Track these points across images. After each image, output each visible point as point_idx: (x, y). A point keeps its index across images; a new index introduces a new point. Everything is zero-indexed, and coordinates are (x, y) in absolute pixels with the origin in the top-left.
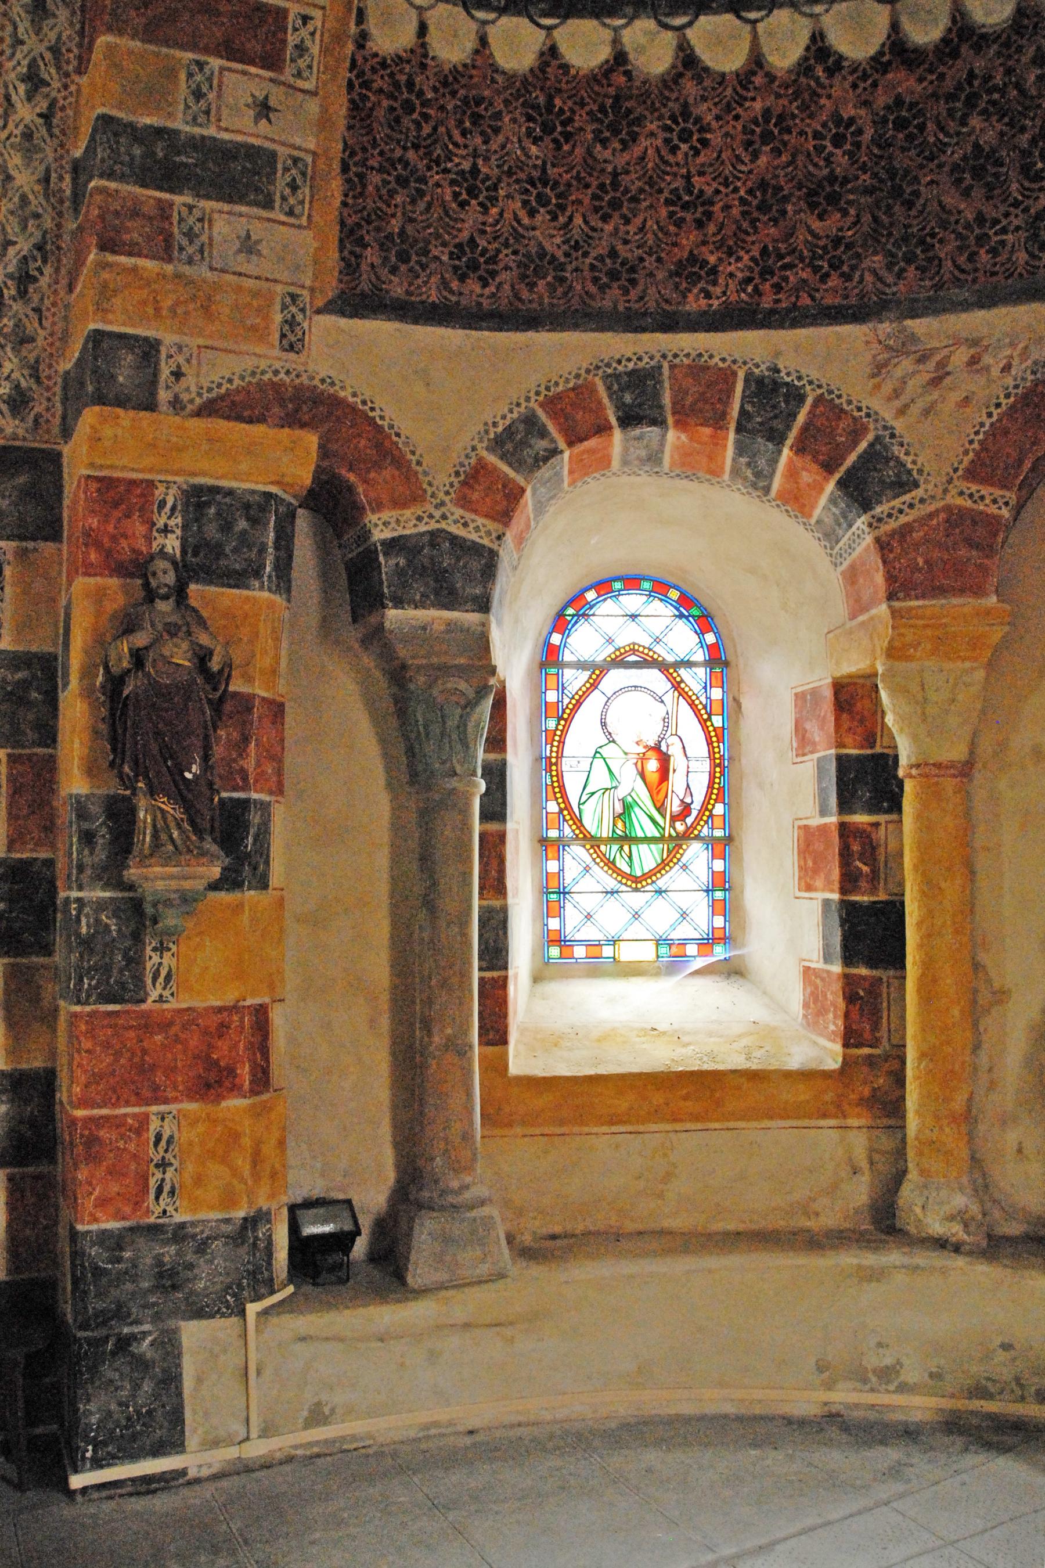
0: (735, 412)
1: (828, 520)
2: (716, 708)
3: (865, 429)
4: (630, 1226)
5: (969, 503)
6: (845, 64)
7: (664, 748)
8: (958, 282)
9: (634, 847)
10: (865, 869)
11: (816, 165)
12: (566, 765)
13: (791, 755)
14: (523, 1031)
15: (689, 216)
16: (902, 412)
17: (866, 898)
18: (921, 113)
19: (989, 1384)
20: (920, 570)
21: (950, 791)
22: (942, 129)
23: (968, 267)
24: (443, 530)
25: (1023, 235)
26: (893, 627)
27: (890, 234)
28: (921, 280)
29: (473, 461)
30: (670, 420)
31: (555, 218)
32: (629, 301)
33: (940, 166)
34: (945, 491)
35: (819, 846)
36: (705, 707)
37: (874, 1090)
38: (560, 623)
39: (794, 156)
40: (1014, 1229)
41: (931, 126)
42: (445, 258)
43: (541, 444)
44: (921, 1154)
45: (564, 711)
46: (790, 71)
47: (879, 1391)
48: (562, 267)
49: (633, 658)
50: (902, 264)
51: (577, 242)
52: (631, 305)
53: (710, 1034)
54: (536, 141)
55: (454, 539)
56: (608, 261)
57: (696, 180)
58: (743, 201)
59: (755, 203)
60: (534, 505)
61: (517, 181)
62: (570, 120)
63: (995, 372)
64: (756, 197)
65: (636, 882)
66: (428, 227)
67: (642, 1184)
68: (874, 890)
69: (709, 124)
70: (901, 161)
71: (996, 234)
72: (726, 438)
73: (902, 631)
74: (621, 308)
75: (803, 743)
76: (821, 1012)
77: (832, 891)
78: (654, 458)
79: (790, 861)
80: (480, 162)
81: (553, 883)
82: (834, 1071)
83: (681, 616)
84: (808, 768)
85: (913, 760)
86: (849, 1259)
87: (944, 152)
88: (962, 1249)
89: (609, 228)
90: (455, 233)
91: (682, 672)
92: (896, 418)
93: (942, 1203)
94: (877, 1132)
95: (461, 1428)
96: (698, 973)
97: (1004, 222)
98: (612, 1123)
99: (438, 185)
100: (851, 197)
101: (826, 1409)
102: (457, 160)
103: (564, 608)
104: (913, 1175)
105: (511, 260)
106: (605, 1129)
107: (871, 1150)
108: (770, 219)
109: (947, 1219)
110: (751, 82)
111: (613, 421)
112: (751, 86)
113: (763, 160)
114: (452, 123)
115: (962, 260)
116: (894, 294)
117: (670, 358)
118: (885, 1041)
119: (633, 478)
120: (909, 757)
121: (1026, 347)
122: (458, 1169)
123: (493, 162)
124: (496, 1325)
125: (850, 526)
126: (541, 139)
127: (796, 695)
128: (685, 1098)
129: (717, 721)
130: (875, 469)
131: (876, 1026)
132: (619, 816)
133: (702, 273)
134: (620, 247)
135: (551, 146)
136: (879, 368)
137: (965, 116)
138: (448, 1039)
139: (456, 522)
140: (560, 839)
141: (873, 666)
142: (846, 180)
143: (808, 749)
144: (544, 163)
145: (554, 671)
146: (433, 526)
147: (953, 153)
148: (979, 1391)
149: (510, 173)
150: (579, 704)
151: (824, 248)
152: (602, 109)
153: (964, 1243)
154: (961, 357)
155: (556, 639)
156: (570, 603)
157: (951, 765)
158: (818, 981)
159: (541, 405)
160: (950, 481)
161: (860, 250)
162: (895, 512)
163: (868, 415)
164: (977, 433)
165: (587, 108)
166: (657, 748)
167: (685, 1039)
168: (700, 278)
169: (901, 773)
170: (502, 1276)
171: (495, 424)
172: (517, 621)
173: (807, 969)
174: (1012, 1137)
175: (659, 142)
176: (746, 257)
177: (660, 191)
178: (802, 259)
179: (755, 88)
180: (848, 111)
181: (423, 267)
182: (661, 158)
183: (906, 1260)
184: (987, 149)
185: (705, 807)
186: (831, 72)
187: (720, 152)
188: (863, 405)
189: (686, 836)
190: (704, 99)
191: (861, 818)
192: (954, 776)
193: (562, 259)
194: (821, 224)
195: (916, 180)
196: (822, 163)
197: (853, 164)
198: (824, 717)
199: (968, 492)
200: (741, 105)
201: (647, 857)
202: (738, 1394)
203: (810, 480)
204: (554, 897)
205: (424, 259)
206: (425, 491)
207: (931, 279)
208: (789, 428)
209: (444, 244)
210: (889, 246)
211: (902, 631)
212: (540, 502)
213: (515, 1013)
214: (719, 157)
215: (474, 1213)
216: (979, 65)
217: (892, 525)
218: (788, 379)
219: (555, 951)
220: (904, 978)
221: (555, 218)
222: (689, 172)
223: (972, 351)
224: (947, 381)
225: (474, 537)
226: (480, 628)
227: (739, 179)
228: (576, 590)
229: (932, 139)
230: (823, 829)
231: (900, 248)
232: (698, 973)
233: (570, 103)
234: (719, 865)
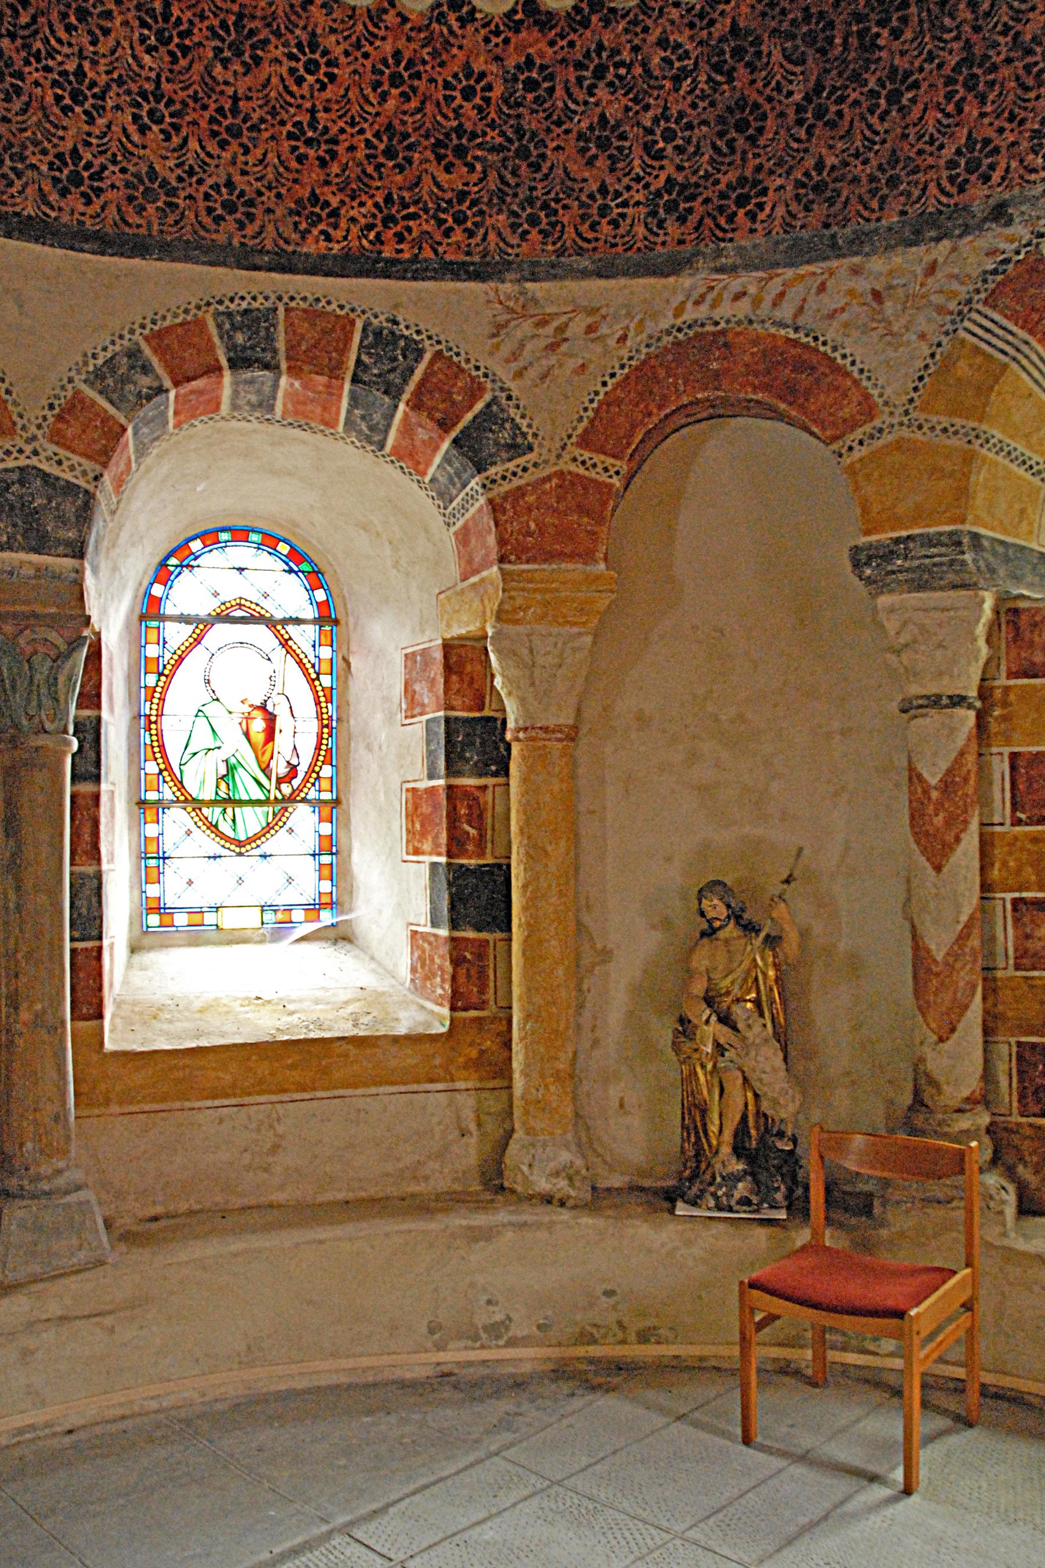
0: (351, 364)
1: (443, 480)
2: (325, 667)
3: (481, 389)
4: (237, 1202)
5: (581, 471)
6: (478, 16)
7: (270, 708)
8: (580, 252)
9: (237, 810)
10: (473, 832)
11: (445, 116)
12: (166, 723)
13: (400, 717)
14: (119, 1004)
15: (311, 153)
16: (519, 374)
17: (473, 862)
18: (551, 77)
19: (595, 1331)
20: (530, 534)
21: (556, 754)
22: (570, 95)
23: (590, 235)
24: (35, 468)
25: (643, 210)
26: (504, 591)
27: (515, 195)
28: (544, 244)
29: (69, 394)
30: (284, 366)
31: (168, 138)
32: (244, 237)
33: (567, 132)
34: (559, 456)
35: (426, 809)
36: (313, 666)
37: (482, 1052)
38: (163, 574)
39: (423, 103)
40: (617, 1181)
41: (559, 92)
42: (44, 168)
43: (145, 382)
44: (527, 1112)
45: (165, 667)
46: (421, 14)
47: (490, 1347)
48: (172, 192)
49: (239, 613)
50: (526, 226)
51: (191, 167)
52: (246, 241)
53: (317, 1002)
54: (149, 50)
55: (45, 476)
56: (224, 190)
57: (321, 115)
58: (368, 144)
59: (382, 147)
60: (136, 446)
61: (129, 92)
62: (188, 33)
63: (612, 342)
64: (382, 141)
65: (240, 845)
66: (25, 130)
67: (247, 1158)
68: (482, 854)
69: (337, 59)
70: (531, 123)
71: (617, 206)
72: (342, 387)
73: (513, 593)
74: (236, 242)
75: (413, 705)
76: (429, 977)
77: (439, 854)
78: (266, 405)
79: (398, 824)
80: (87, 65)
81: (152, 848)
82: (442, 1035)
83: (291, 571)
84: (418, 729)
85: (521, 723)
86: (459, 1220)
87: (571, 119)
88: (568, 1204)
89: (226, 155)
90: (55, 141)
91: (291, 628)
92: (514, 379)
93: (549, 1160)
94: (485, 1094)
95: (59, 1429)
96: (303, 939)
97: (626, 196)
98: (215, 1097)
99: (37, 84)
100: (479, 153)
101: (438, 1369)
102: (59, 58)
103: (167, 558)
104: (519, 1134)
105: (119, 179)
106: (209, 1103)
107: (478, 1113)
108: (395, 166)
109: (551, 1175)
110: (382, 20)
111: (224, 363)
112: (382, 25)
113: (391, 104)
114: (55, 16)
115: (584, 228)
116: (517, 255)
117: (286, 299)
118: (492, 1003)
119: (244, 424)
120: (516, 721)
121: (642, 321)
122: (47, 1152)
123: (102, 68)
124: (96, 1315)
125: (464, 486)
126: (156, 49)
127: (406, 655)
128: (293, 1067)
129: (326, 681)
130: (491, 430)
131: (482, 991)
132: (222, 778)
133: (324, 215)
134: (237, 178)
135: (167, 59)
136: (498, 329)
137: (593, 86)
138: (37, 1016)
139: (49, 459)
140: (159, 802)
141: (483, 629)
142: (474, 135)
143: (418, 710)
144: (159, 76)
145: (154, 624)
146: (23, 462)
147: (579, 121)
148: (586, 1338)
149: (120, 82)
150: (181, 659)
151: (449, 202)
152: (224, 25)
153: (569, 1197)
154: (578, 326)
155: (157, 590)
156: (172, 554)
157: (558, 729)
158: (426, 945)
159: (147, 339)
160: (563, 448)
161: (484, 208)
162: (508, 475)
163: (486, 375)
164: (592, 401)
165: (206, 23)
166: (263, 708)
167: (291, 1007)
168: (320, 220)
169: (508, 736)
170: (100, 1263)
171: (94, 356)
172: (115, 569)
173: (415, 933)
174: (614, 1093)
175: (284, 70)
176: (370, 203)
177: (283, 123)
178: (426, 211)
179: (387, 28)
180: (478, 65)
181: (19, 175)
182: (286, 87)
183: (514, 1218)
184: (612, 122)
185: (311, 769)
186: (463, 22)
187: (347, 90)
188: (481, 364)
189: (291, 799)
190: (333, 31)
191: (469, 782)
192: (560, 740)
193: (174, 184)
194: (447, 177)
195: (543, 143)
196: (451, 115)
197: (481, 119)
198: (433, 680)
199: (580, 459)
200: (371, 44)
201: (251, 820)
202: (350, 1363)
203: (426, 437)
204: (152, 863)
205: (19, 166)
206: (14, 424)
207: (554, 243)
208: (405, 381)
209: (44, 152)
210: (515, 208)
211: (513, 593)
212: (142, 443)
213: (111, 985)
214: (345, 95)
215: (68, 1199)
216: (607, 39)
217: (506, 487)
218: (406, 333)
219: (154, 920)
220: (510, 940)
221: (168, 138)
222: (314, 106)
223: (590, 320)
224: (564, 347)
225: (68, 476)
226: (73, 575)
227: (366, 120)
228: (181, 539)
229: (560, 104)
230: (431, 791)
231: (524, 209)
232: (303, 939)
233: (189, 14)
234: (326, 829)
